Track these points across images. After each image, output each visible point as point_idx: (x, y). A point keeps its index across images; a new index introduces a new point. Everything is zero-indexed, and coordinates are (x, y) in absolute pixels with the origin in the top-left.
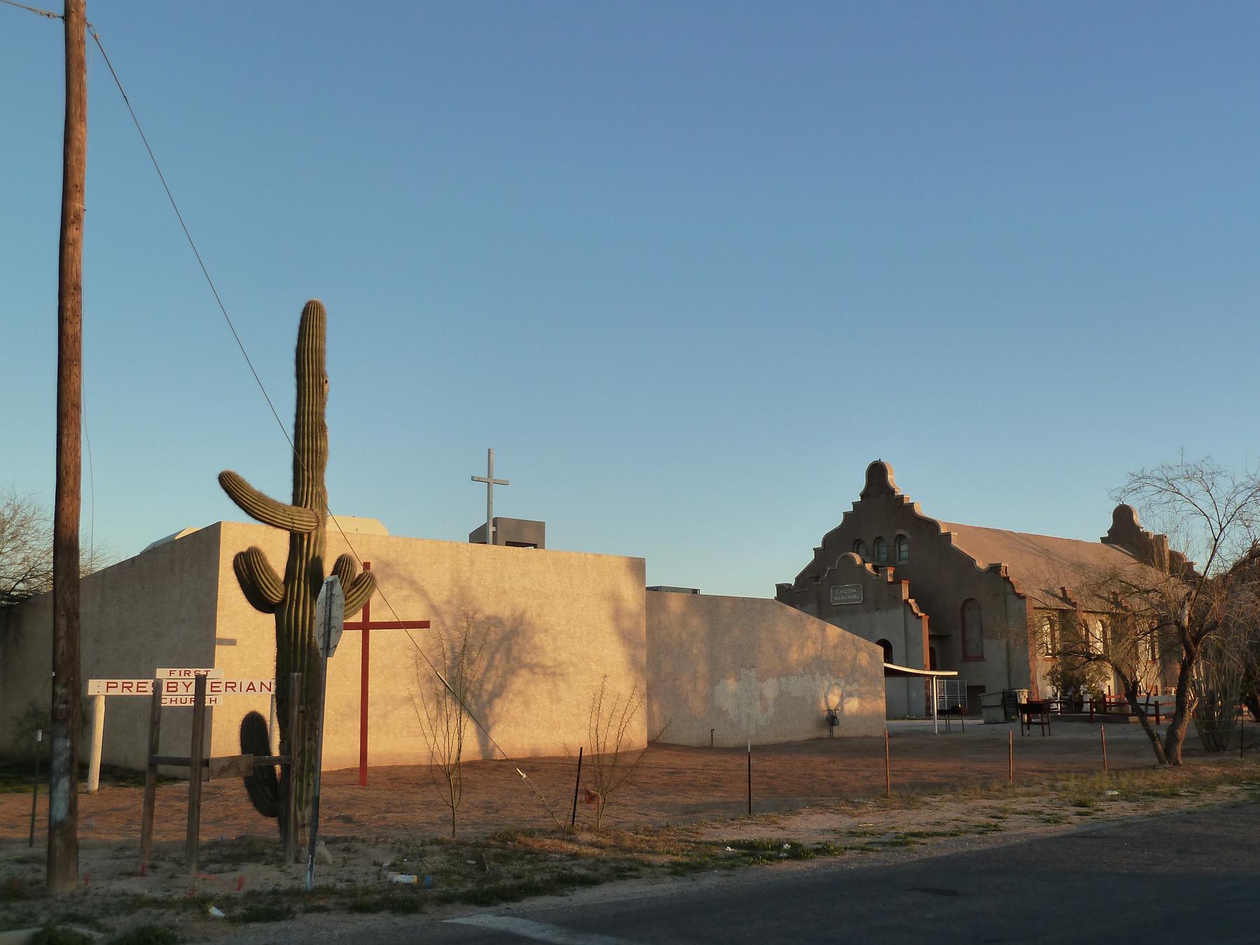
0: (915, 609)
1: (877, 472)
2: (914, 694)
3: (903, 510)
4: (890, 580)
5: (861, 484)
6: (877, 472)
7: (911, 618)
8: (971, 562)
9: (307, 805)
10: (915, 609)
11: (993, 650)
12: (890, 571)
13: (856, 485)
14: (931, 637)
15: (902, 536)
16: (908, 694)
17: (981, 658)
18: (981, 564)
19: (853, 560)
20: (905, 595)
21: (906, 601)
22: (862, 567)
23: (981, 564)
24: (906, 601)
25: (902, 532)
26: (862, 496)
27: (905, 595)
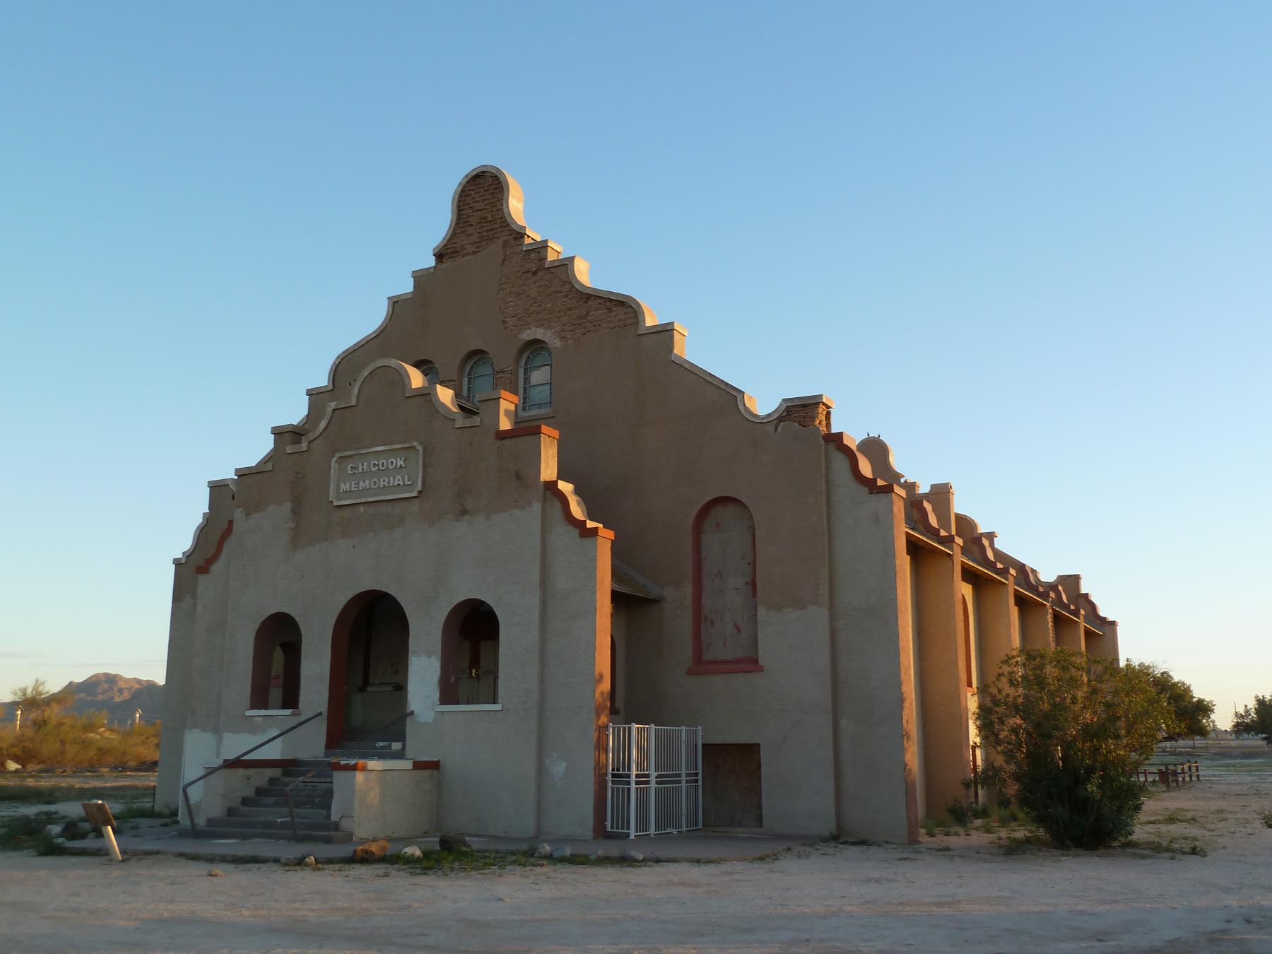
0: (577, 510)
1: (482, 194)
2: (558, 768)
3: (545, 276)
4: (505, 424)
5: (437, 223)
6: (482, 194)
7: (564, 536)
8: (730, 397)
9: (1031, 831)
10: (577, 510)
11: (791, 643)
12: (507, 404)
13: (417, 233)
14: (616, 597)
15: (535, 346)
16: (540, 764)
17: (751, 663)
18: (763, 401)
19: (403, 379)
20: (548, 471)
21: (551, 486)
22: (426, 395)
23: (763, 401)
24: (551, 486)
25: (539, 333)
26: (440, 256)
27: (548, 471)
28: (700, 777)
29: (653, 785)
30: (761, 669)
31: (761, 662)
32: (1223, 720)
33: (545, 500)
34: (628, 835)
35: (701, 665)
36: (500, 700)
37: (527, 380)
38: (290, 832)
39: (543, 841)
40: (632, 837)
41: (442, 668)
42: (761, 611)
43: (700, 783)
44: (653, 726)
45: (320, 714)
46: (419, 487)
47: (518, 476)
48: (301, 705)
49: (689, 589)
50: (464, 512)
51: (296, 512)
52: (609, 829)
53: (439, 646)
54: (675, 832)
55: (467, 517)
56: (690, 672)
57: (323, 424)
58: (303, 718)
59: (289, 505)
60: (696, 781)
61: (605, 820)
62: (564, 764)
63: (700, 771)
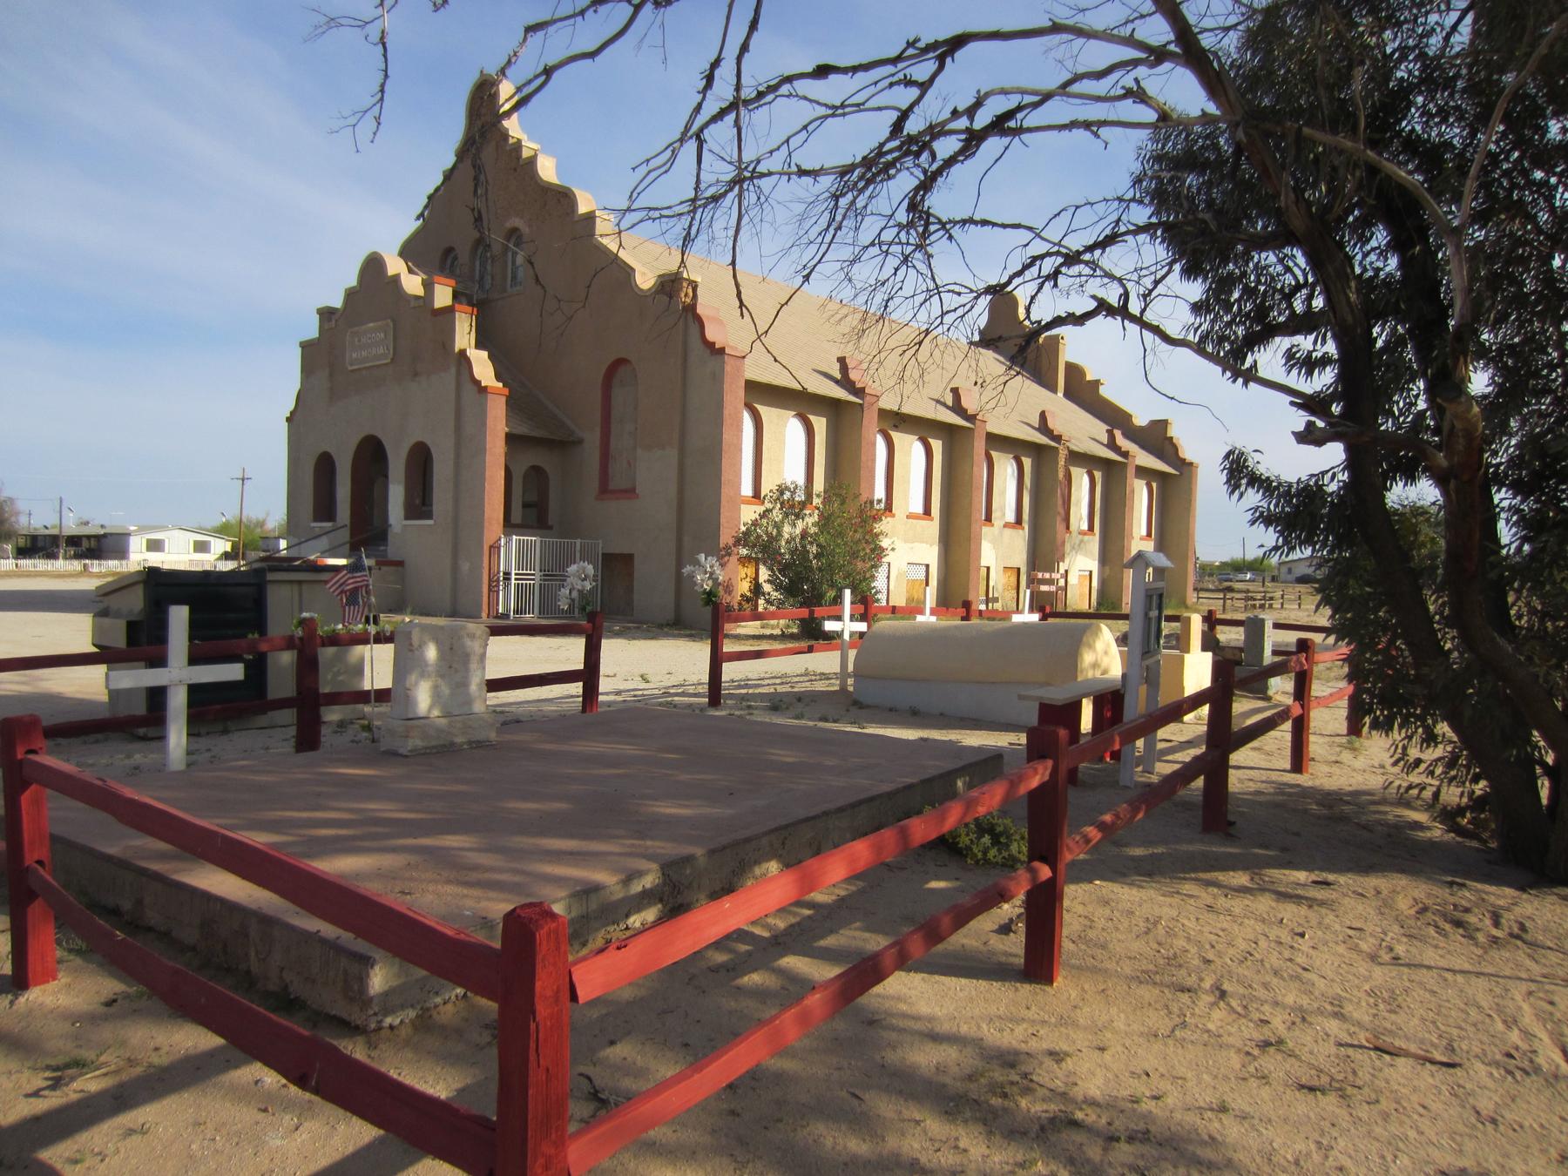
17: (630, 492)
30: (637, 496)
35: (605, 490)
50: (416, 374)
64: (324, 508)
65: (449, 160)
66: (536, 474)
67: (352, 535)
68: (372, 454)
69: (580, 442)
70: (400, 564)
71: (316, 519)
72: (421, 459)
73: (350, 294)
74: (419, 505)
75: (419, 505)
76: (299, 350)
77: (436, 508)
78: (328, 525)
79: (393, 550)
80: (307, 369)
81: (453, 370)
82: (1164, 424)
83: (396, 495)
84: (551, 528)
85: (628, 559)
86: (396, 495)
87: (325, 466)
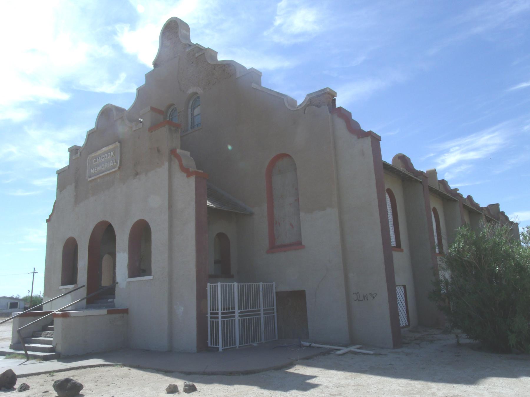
2: (180, 310)
17: (298, 245)
28: (275, 310)
29: (220, 320)
30: (304, 247)
31: (303, 244)
32: (42, 296)
33: (170, 161)
34: (218, 349)
35: (274, 247)
36: (152, 274)
37: (192, 114)
38: (29, 353)
39: (438, 282)
40: (220, 350)
41: (129, 258)
42: (302, 214)
43: (275, 314)
44: (236, 284)
45: (84, 286)
46: (118, 165)
47: (159, 151)
48: (78, 283)
49: (265, 206)
50: (137, 174)
51: (76, 187)
52: (209, 345)
53: (127, 247)
54: (255, 344)
55: (138, 176)
56: (268, 252)
57: (105, 149)
58: (79, 286)
59: (74, 184)
60: (274, 313)
61: (207, 340)
62: (183, 308)
63: (275, 307)
64: (69, 275)
65: (50, 210)
66: (222, 237)
67: (88, 293)
68: (104, 236)
69: (252, 214)
70: (125, 311)
71: (63, 284)
72: (141, 233)
73: (91, 135)
74: (140, 267)
75: (140, 267)
76: (68, 154)
77: (154, 267)
78: (72, 287)
79: (120, 300)
80: (61, 186)
81: (166, 165)
82: (497, 205)
83: (122, 259)
84: (232, 277)
85: (299, 296)
86: (122, 259)
87: (70, 250)
